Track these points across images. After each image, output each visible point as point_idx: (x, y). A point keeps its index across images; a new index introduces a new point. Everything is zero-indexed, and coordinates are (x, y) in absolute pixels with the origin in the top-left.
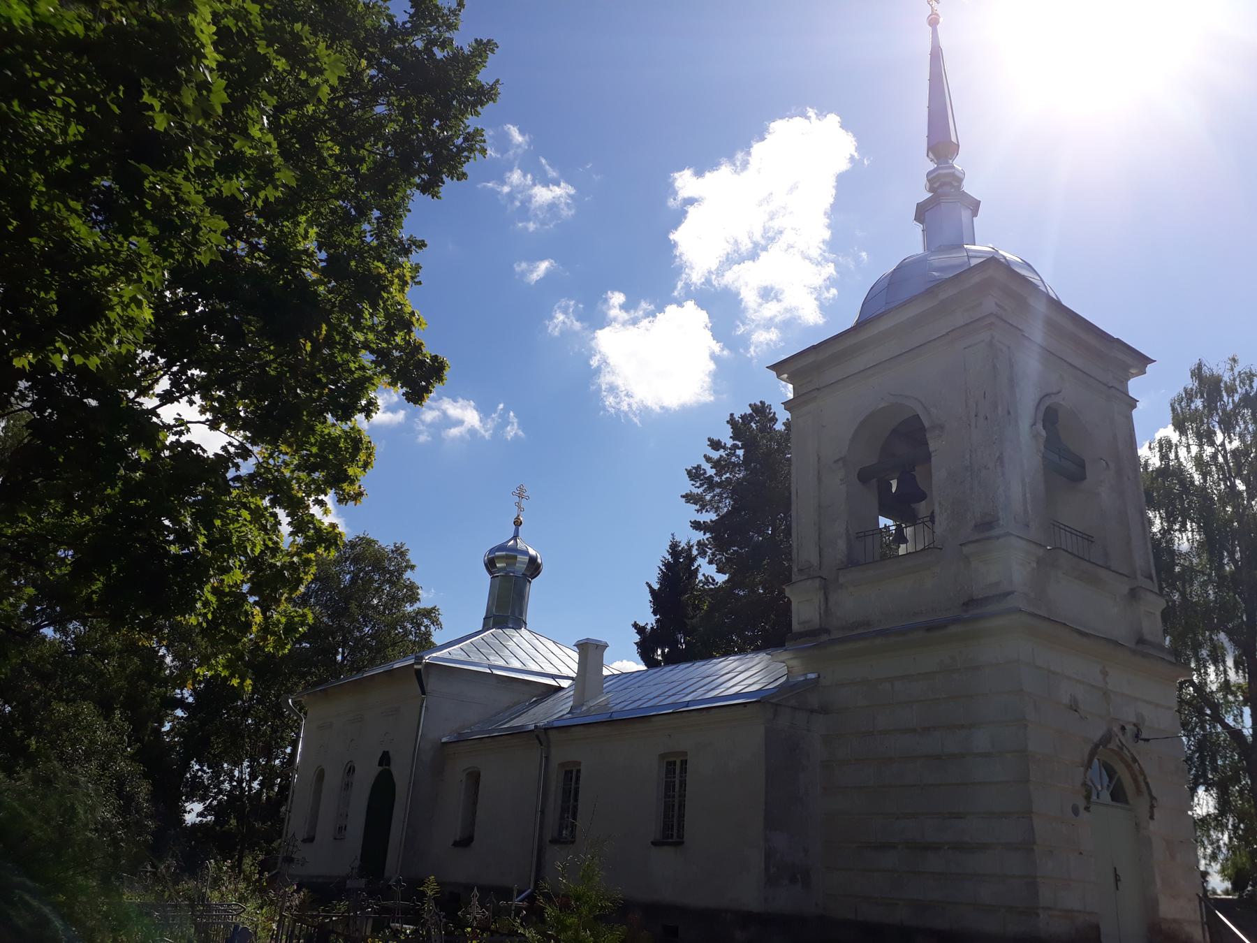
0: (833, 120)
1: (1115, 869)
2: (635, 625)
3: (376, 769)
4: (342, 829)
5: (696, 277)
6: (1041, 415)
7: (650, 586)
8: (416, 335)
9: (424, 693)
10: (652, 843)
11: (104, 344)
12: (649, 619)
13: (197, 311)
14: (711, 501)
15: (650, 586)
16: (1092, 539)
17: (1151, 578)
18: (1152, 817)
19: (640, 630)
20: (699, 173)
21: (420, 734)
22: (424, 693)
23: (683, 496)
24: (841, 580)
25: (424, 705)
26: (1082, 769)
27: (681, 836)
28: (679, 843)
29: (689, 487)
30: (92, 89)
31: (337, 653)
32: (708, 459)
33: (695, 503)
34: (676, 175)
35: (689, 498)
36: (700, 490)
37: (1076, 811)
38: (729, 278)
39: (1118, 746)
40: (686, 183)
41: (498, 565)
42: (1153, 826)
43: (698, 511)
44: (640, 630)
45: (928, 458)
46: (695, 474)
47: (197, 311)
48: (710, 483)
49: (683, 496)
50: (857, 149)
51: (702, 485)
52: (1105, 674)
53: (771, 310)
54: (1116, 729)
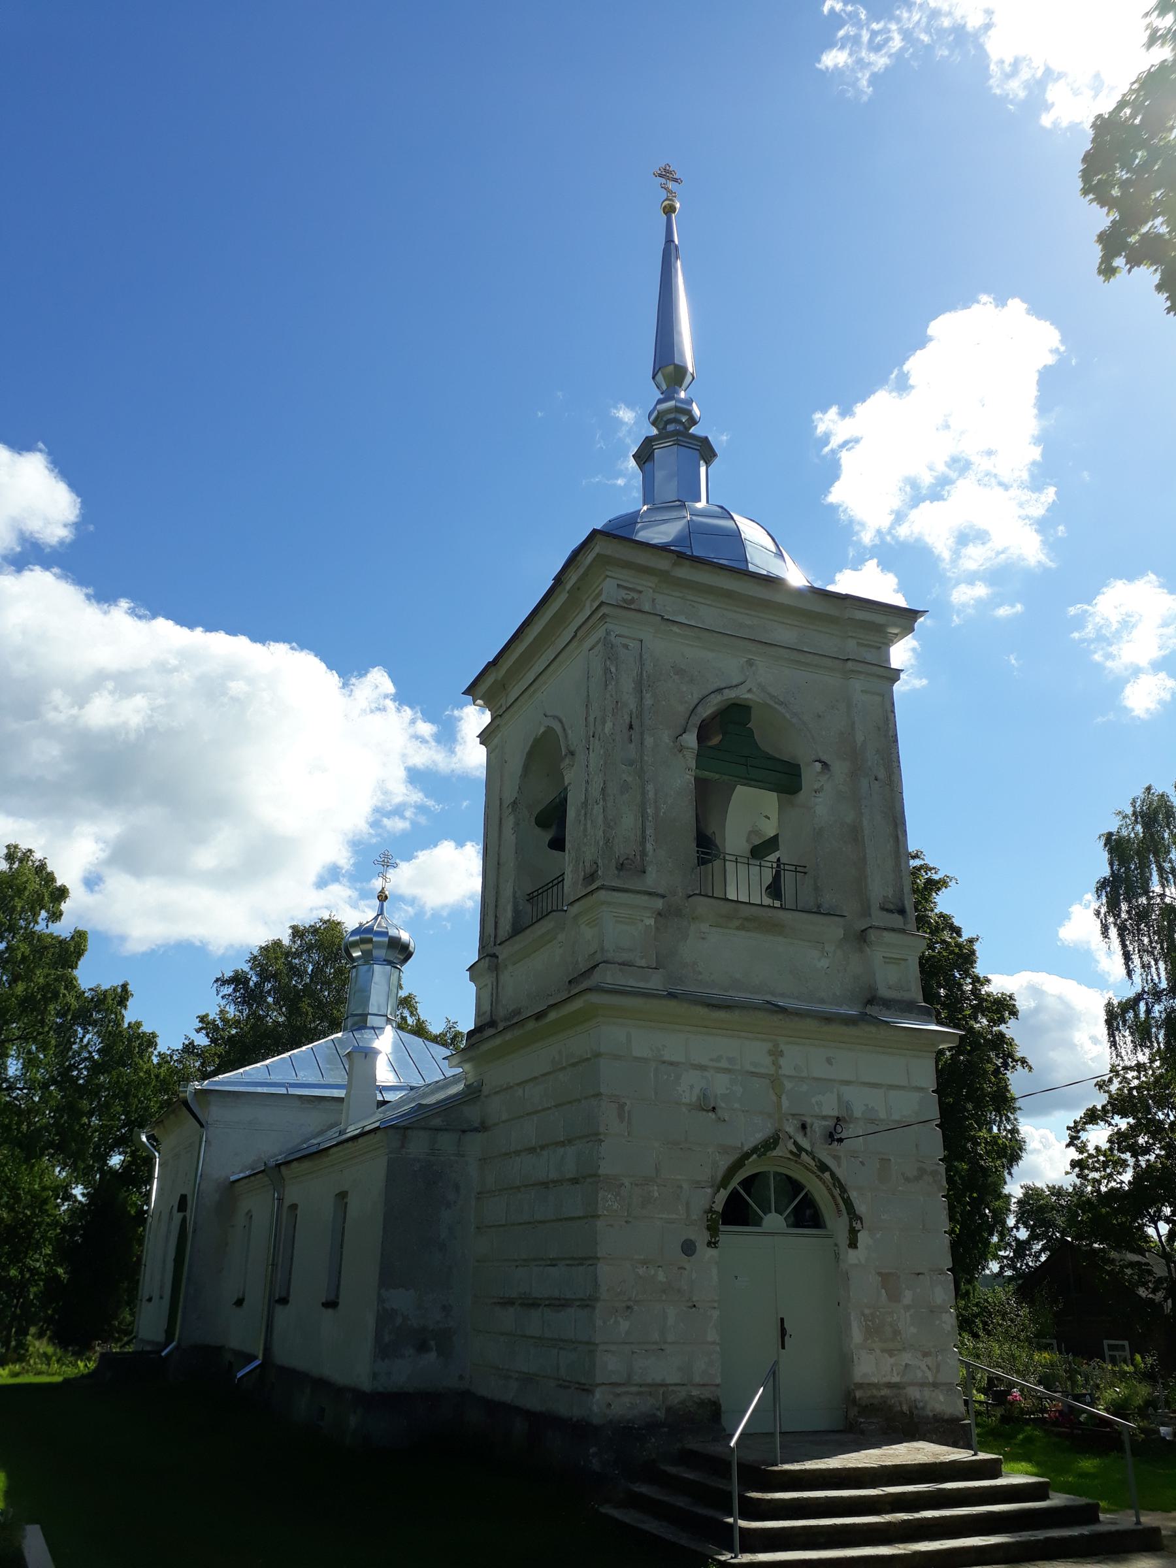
0: (1016, 306)
1: (782, 1320)
5: (867, 538)
9: (202, 1126)
10: (323, 1304)
11: (1127, 619)
16: (805, 870)
17: (902, 912)
18: (853, 1244)
20: (846, 412)
21: (199, 1174)
22: (202, 1126)
25: (204, 1139)
26: (709, 1190)
31: (1167, 948)
34: (817, 416)
37: (688, 1248)
38: (903, 531)
39: (791, 1152)
40: (829, 422)
41: (360, 953)
42: (853, 1257)
50: (1063, 341)
52: (776, 1053)
53: (975, 557)
54: (790, 1128)
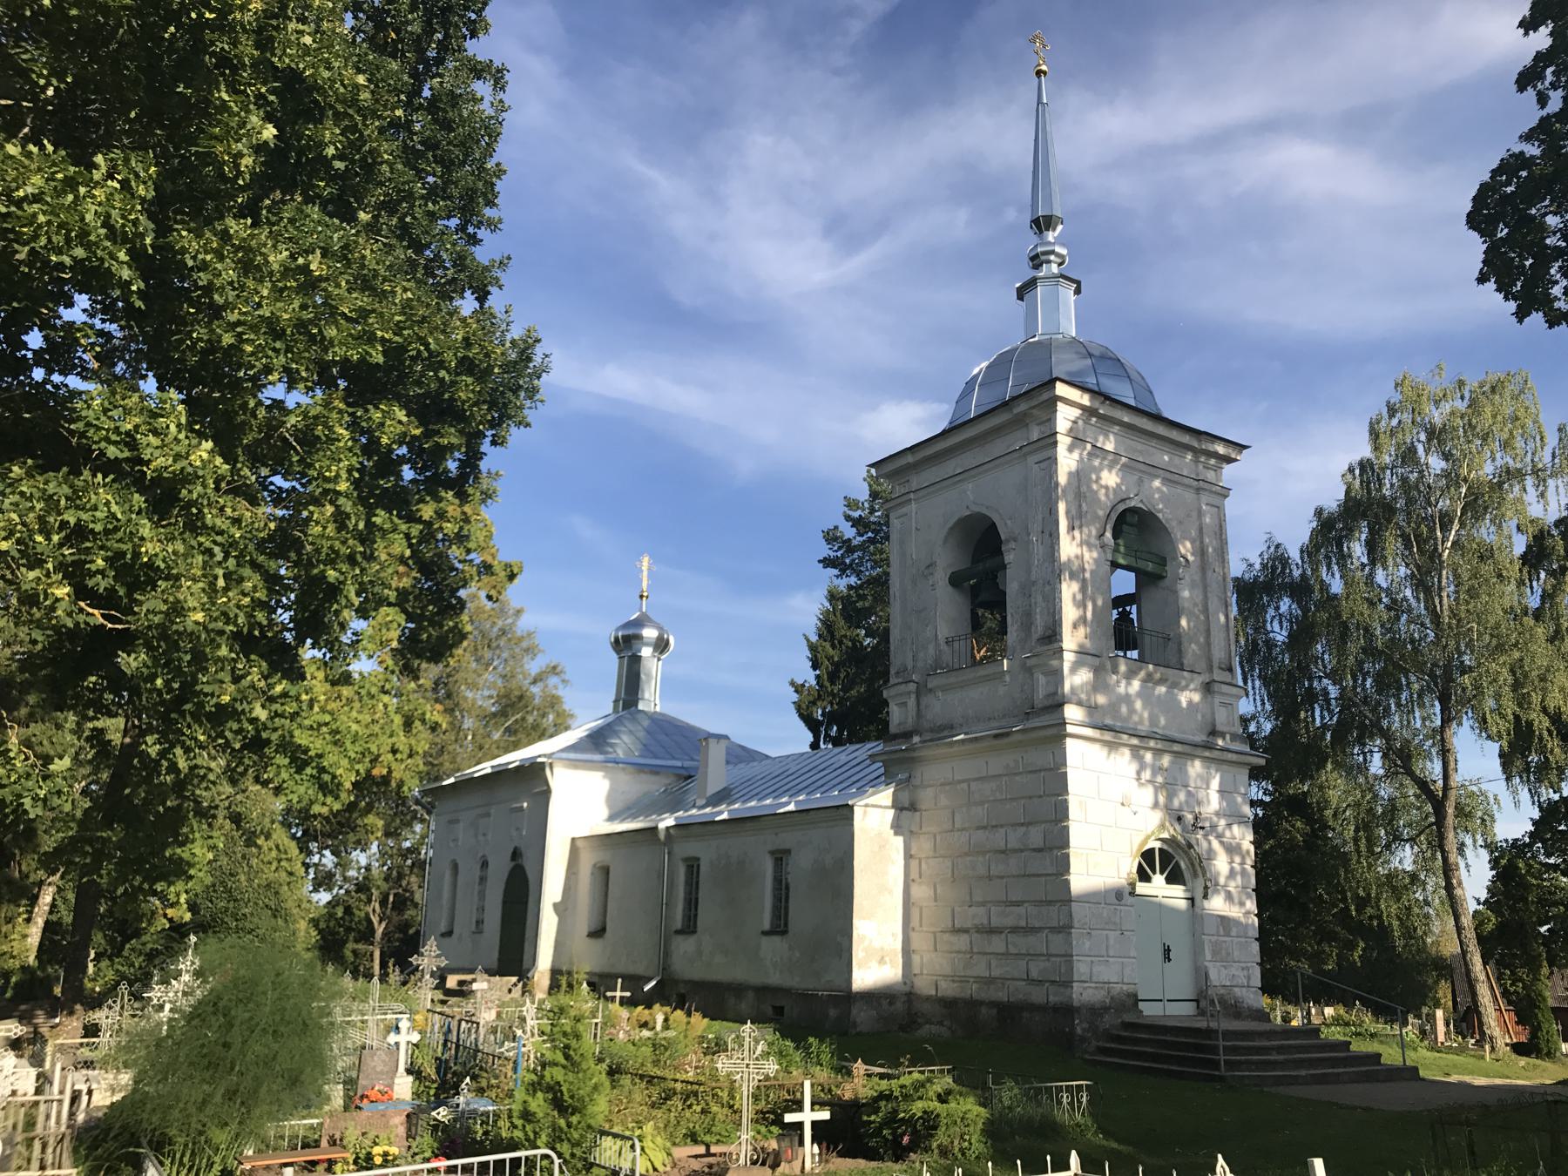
2: (792, 683)
3: (509, 865)
4: (479, 922)
6: (1114, 516)
7: (808, 640)
8: (496, 301)
12: (808, 676)
13: (143, 307)
14: (851, 564)
15: (808, 640)
19: (798, 688)
23: (820, 561)
24: (929, 686)
27: (786, 924)
28: (784, 932)
29: (825, 551)
30: (10, 305)
32: (848, 518)
33: (835, 567)
35: (827, 562)
36: (839, 554)
43: (837, 577)
44: (798, 688)
45: (1004, 567)
46: (831, 537)
47: (143, 307)
48: (848, 547)
49: (820, 561)
51: (840, 548)
